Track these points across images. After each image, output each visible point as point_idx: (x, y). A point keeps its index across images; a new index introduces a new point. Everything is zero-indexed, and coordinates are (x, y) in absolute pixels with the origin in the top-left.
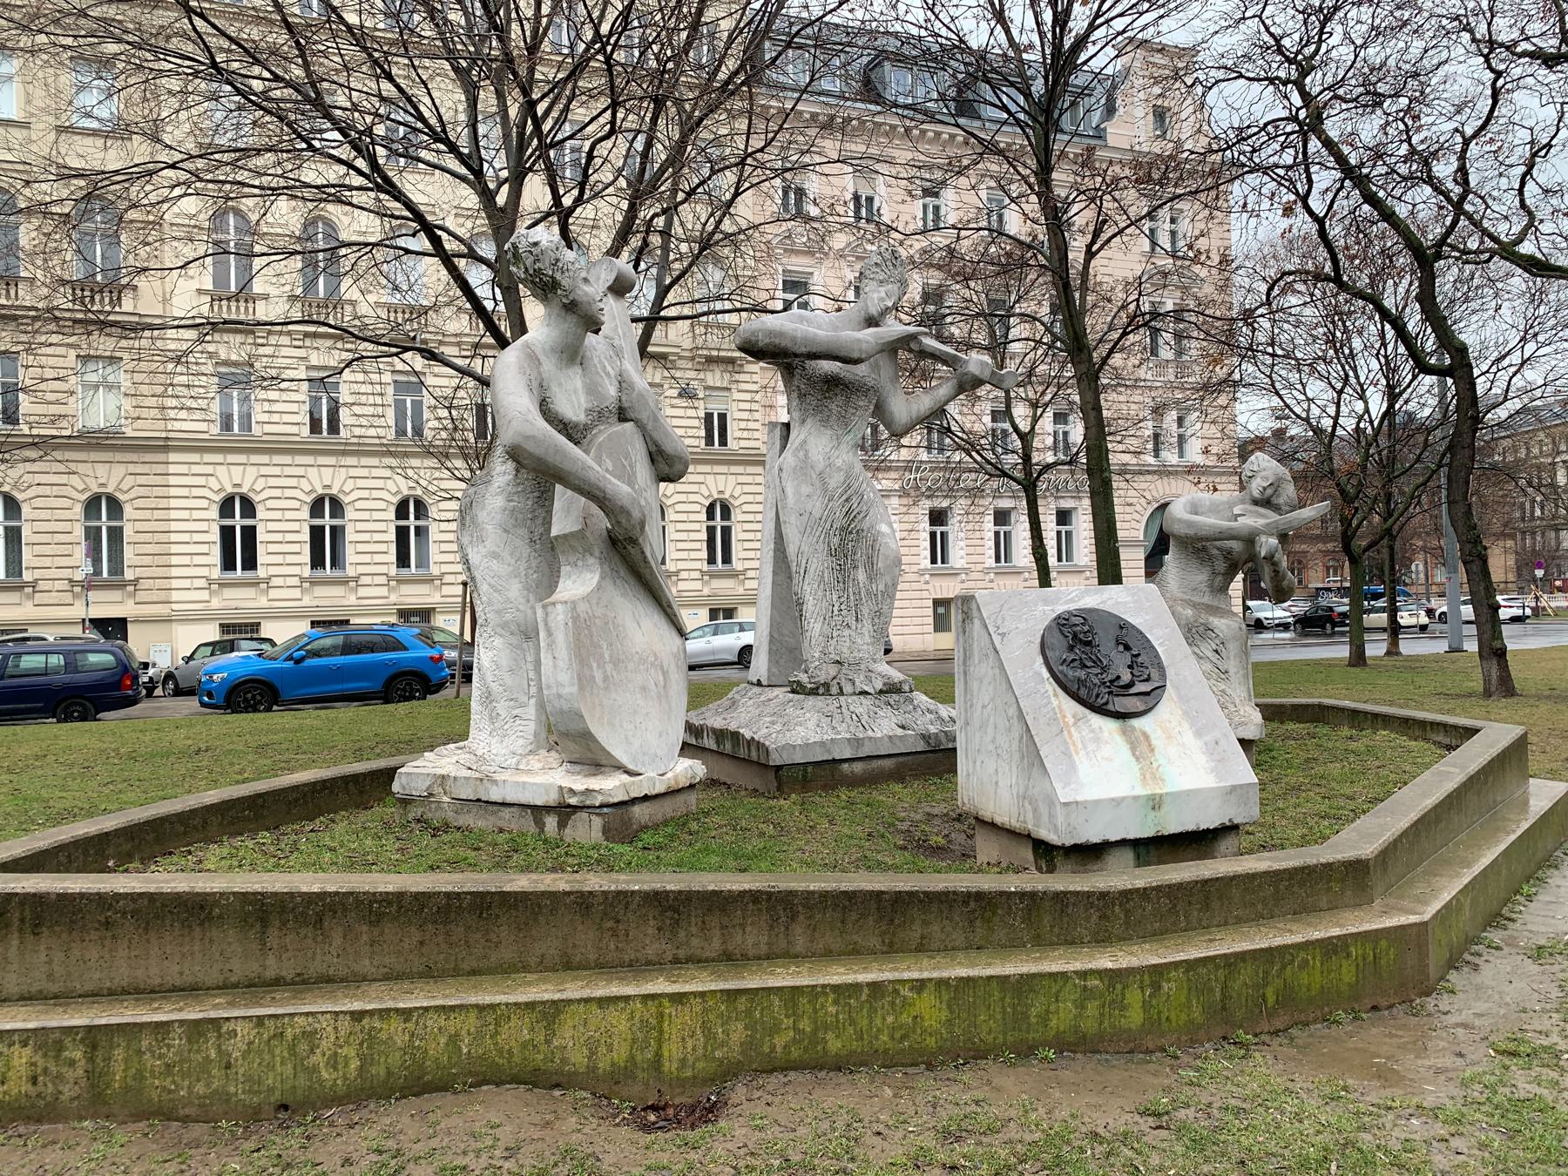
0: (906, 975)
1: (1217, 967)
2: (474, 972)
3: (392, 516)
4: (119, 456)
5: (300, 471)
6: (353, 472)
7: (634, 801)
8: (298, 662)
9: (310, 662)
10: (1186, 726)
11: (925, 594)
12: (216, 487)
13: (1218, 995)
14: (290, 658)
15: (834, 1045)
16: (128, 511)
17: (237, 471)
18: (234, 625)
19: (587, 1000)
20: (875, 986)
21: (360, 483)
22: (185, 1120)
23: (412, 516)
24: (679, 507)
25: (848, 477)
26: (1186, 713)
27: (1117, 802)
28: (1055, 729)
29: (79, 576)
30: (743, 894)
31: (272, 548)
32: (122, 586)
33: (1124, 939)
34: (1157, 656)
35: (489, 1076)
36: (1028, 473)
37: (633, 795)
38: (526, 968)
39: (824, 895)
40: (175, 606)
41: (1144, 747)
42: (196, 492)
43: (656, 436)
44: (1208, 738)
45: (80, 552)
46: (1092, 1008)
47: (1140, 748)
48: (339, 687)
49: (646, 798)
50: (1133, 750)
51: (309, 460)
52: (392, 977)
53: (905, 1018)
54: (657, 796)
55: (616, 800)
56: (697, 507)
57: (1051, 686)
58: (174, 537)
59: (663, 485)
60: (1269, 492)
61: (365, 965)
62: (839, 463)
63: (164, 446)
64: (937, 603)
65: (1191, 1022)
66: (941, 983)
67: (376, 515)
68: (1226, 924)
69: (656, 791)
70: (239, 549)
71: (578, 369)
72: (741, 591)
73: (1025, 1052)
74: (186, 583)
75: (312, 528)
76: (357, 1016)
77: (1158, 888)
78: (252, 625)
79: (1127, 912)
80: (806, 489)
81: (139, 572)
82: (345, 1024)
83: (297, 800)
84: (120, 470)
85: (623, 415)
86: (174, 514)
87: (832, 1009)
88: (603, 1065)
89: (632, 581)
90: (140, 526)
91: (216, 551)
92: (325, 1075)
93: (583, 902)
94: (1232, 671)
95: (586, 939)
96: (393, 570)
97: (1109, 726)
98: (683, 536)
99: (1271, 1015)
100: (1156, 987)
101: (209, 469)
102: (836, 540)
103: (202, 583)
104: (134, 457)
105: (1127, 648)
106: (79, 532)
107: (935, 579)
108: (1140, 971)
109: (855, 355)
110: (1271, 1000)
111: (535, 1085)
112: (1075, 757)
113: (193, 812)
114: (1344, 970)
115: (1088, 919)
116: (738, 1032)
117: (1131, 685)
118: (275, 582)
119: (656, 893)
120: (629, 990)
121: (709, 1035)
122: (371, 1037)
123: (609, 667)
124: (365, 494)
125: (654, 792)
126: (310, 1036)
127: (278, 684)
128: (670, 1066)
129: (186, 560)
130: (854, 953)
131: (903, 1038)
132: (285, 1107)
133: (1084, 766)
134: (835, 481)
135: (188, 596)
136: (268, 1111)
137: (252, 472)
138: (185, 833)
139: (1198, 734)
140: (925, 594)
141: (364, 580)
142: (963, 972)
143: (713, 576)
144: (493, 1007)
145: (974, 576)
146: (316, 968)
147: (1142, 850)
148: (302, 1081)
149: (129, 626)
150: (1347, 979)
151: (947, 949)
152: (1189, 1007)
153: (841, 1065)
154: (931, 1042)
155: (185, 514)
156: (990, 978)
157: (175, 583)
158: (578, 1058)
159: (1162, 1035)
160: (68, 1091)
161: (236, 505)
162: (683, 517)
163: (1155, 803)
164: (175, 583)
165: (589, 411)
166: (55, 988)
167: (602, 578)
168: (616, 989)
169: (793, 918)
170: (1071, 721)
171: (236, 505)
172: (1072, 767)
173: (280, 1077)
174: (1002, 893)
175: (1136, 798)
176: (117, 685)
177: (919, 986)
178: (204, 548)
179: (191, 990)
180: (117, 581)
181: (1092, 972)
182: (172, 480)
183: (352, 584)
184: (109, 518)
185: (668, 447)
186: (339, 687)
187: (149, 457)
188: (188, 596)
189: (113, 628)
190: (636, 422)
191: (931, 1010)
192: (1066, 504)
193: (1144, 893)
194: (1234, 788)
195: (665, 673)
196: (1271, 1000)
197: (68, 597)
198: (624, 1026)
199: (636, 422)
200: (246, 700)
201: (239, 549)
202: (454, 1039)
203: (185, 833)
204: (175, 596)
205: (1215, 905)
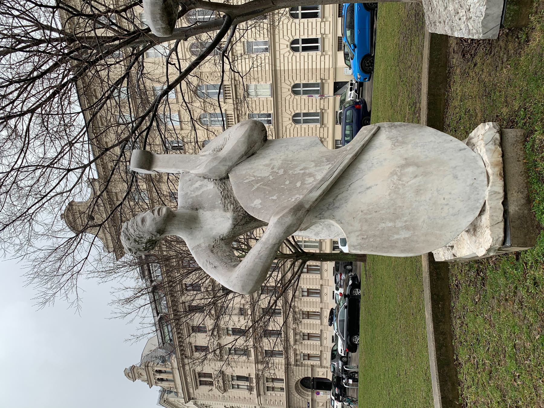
4: (279, 85)
5: (282, 56)
6: (281, 36)
7: (506, 212)
8: (355, 46)
9: (356, 42)
12: (288, 53)
16: (297, 82)
17: (282, 46)
18: (338, 46)
23: (297, 12)
29: (319, 125)
31: (310, 33)
32: (323, 84)
37: (501, 218)
40: (331, 67)
42: (290, 60)
43: (235, 159)
45: (312, 125)
48: (367, 30)
49: (505, 203)
51: (278, 53)
54: (502, 151)
55: (502, 235)
58: (306, 67)
59: (270, 138)
63: (275, 72)
67: (298, 60)
69: (501, 190)
70: (310, 45)
71: (201, 212)
75: (302, 18)
78: (339, 39)
81: (318, 78)
83: (437, 274)
84: (284, 85)
85: (224, 179)
86: (298, 68)
89: (336, 191)
90: (302, 33)
101: (282, 56)
103: (323, 58)
106: (305, 126)
113: (437, 340)
118: (323, 32)
123: (399, 224)
124: (289, 31)
125: (502, 194)
127: (363, 55)
129: (314, 63)
137: (282, 41)
138: (446, 347)
157: (323, 67)
161: (294, 46)
164: (323, 67)
165: (226, 210)
167: (333, 218)
171: (294, 46)
176: (358, 110)
180: (322, 85)
182: (286, 68)
183: (323, 111)
184: (300, 87)
185: (242, 149)
186: (367, 30)
187: (279, 76)
188: (328, 62)
189: (338, 86)
197: (326, 129)
200: (369, 66)
201: (310, 45)
203: (446, 347)
204: (327, 67)
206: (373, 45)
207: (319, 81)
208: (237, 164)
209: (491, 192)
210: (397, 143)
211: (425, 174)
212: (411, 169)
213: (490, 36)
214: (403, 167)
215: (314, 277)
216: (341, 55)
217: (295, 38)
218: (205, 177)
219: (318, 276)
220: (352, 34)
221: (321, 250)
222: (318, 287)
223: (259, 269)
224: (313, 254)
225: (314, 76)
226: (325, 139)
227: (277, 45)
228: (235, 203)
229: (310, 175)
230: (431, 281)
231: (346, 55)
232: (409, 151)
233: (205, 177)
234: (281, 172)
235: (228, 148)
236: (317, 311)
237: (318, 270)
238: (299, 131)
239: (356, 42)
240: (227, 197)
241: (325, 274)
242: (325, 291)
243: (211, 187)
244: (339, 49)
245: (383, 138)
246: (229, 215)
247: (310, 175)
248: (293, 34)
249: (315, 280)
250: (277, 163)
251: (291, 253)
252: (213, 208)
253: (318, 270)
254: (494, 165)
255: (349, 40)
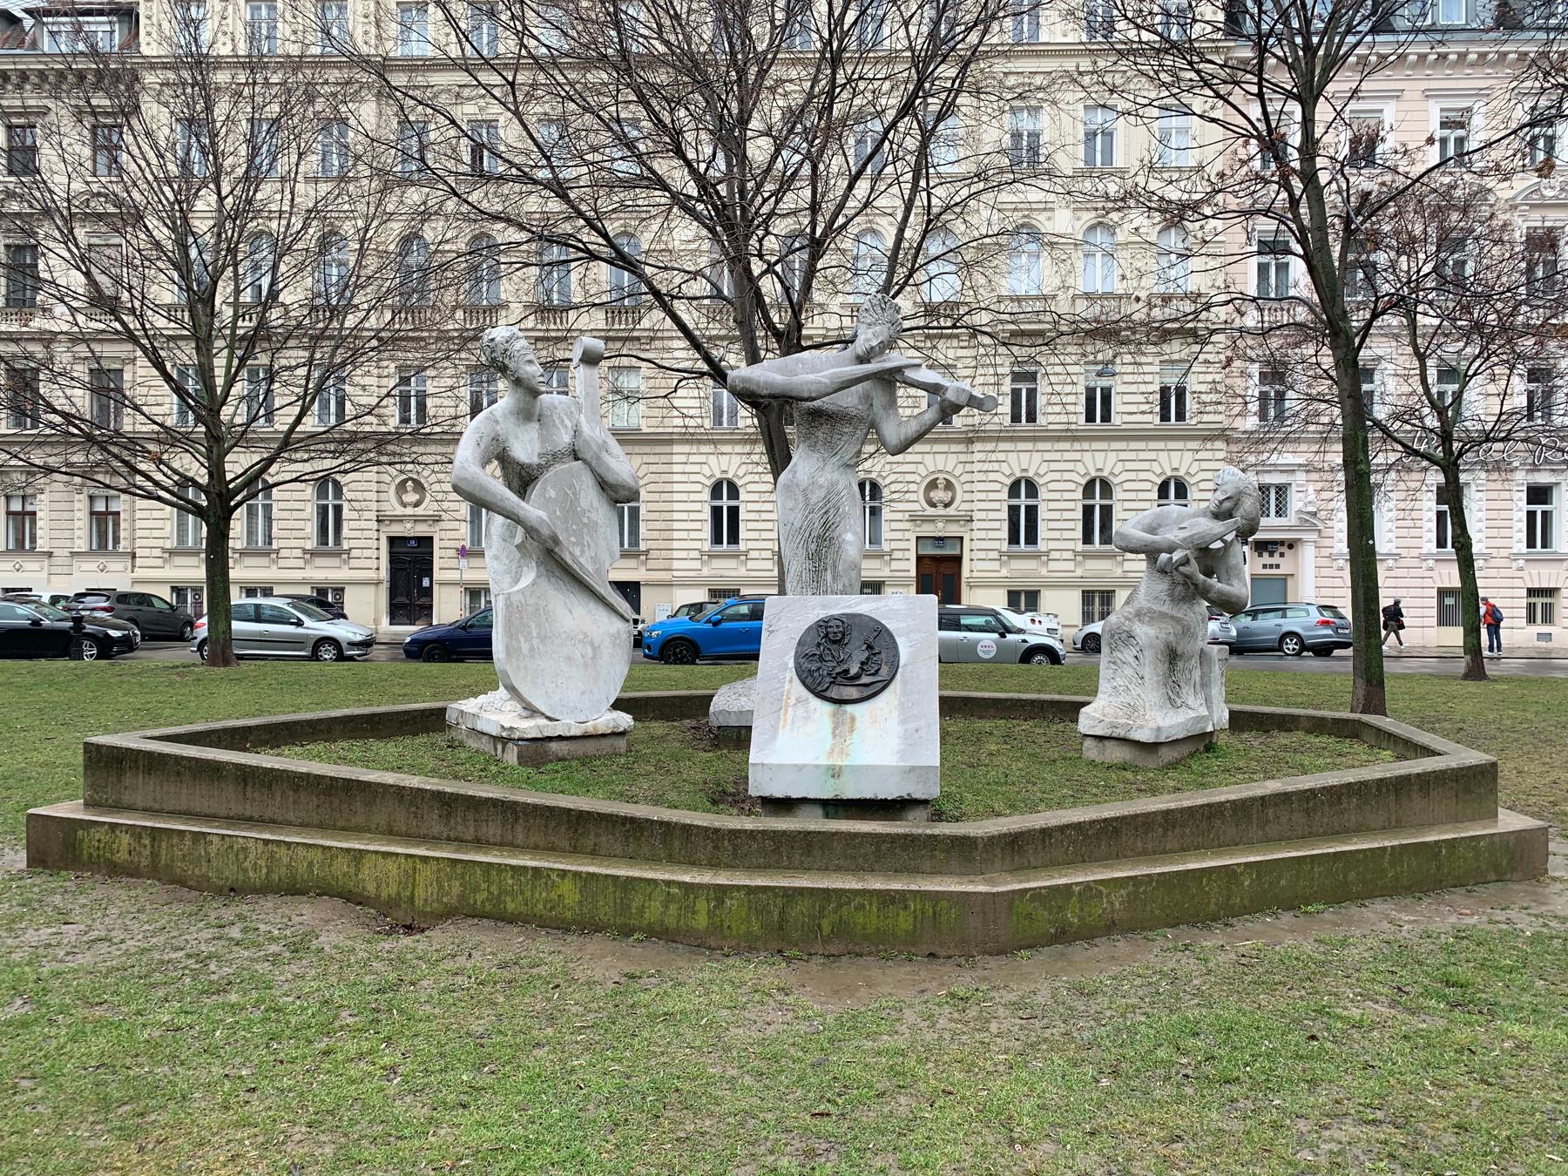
0: (556, 866)
1: (776, 895)
2: (343, 829)
3: (1005, 496)
4: (637, 449)
5: (1152, 455)
7: (550, 739)
8: (715, 624)
9: (725, 625)
10: (896, 713)
11: (1428, 582)
13: (776, 917)
14: (709, 621)
15: (511, 906)
17: (1025, 457)
19: (376, 852)
20: (535, 869)
21: (1129, 466)
22: (191, 888)
24: (1127, 486)
25: (829, 493)
26: (901, 704)
27: (800, 768)
28: (775, 708)
30: (488, 799)
32: (636, 555)
33: (729, 867)
34: (897, 655)
35: (324, 890)
36: (1448, 451)
38: (369, 831)
39: (536, 807)
40: (676, 574)
41: (847, 728)
43: (600, 471)
44: (909, 726)
46: (673, 908)
47: (841, 729)
49: (560, 738)
50: (835, 729)
51: (1160, 445)
52: (304, 825)
53: (553, 895)
56: (1148, 486)
57: (791, 673)
58: (676, 516)
60: (1227, 505)
61: (291, 816)
62: (822, 481)
64: (1532, 592)
65: (750, 933)
66: (577, 874)
67: (693, 497)
68: (827, 869)
69: (572, 733)
71: (536, 425)
72: (1119, 572)
73: (626, 932)
74: (683, 554)
76: (266, 842)
77: (764, 832)
79: (735, 847)
80: (790, 504)
81: (651, 545)
82: (260, 845)
86: (676, 497)
87: (510, 882)
88: (384, 895)
89: (566, 579)
90: (651, 506)
91: (708, 527)
92: (251, 874)
93: (399, 792)
94: (1147, 677)
95: (401, 818)
96: (1005, 546)
97: (827, 708)
98: (1056, 515)
99: (825, 941)
100: (720, 902)
102: (813, 546)
103: (696, 554)
104: (646, 449)
105: (870, 647)
107: (1441, 565)
108: (707, 887)
109: (806, 395)
110: (826, 930)
111: (348, 900)
112: (780, 731)
113: (320, 721)
114: (901, 918)
115: (705, 847)
116: (456, 889)
117: (857, 676)
118: (753, 554)
119: (439, 792)
120: (399, 850)
121: (441, 887)
122: (272, 857)
123: (535, 642)
124: (1057, 476)
126: (244, 849)
128: (419, 903)
130: (552, 849)
131: (552, 909)
132: (232, 889)
133: (784, 734)
134: (817, 496)
135: (686, 565)
136: (226, 890)
139: (903, 722)
140: (1428, 582)
141: (1054, 555)
142: (591, 869)
143: (1087, 556)
144: (330, 848)
145: (1403, 563)
146: (268, 814)
147: (831, 810)
148: (241, 877)
149: (642, 589)
150: (904, 926)
151: (610, 856)
152: (749, 922)
153: (511, 920)
154: (569, 914)
155: (684, 497)
156: (607, 876)
157: (676, 554)
158: (371, 888)
159: (724, 938)
160: (144, 862)
162: (1132, 495)
163: (835, 772)
164: (676, 554)
165: (540, 456)
166: (157, 806)
167: (538, 577)
168: (392, 849)
169: (516, 820)
170: (792, 701)
171: (1098, 486)
172: (774, 737)
173: (231, 873)
174: (647, 820)
175: (817, 766)
177: (563, 874)
178: (697, 525)
179: (210, 817)
181: (674, 882)
185: (610, 478)
187: (658, 449)
188: (686, 565)
190: (584, 461)
191: (569, 892)
192: (1543, 478)
193: (751, 834)
194: (913, 769)
195: (595, 649)
196: (826, 930)
198: (395, 872)
199: (584, 461)
200: (675, 654)
202: (311, 864)
204: (676, 565)
205: (817, 852)
206: (717, 659)
207: (643, 546)
208: (593, 471)
209: (569, 725)
210: (615, 637)
211: (585, 665)
212: (590, 651)
213: (712, 717)
214: (592, 644)
215: (78, 533)
216: (701, 596)
217: (741, 491)
218: (576, 432)
219: (82, 545)
220: (742, 617)
221: (243, 553)
222: (42, 544)
223: (489, 498)
224: (225, 537)
225: (656, 535)
226: (1046, 563)
227: (1179, 445)
228: (547, 466)
229: (582, 552)
230: (397, 713)
231: (698, 607)
232: (607, 650)
233: (576, 432)
234: (585, 520)
235: (611, 462)
236: (39, 542)
237: (102, 545)
238: (296, 515)
239: (725, 625)
240: (555, 458)
241: (91, 565)
242: (31, 565)
243: (565, 438)
244: (714, 593)
245: (619, 625)
246: (535, 460)
247: (582, 552)
248: (1052, 486)
249: (67, 534)
250: (593, 516)
251: (229, 476)
252: (544, 439)
253: (102, 545)
254: (595, 727)
255: (730, 611)
